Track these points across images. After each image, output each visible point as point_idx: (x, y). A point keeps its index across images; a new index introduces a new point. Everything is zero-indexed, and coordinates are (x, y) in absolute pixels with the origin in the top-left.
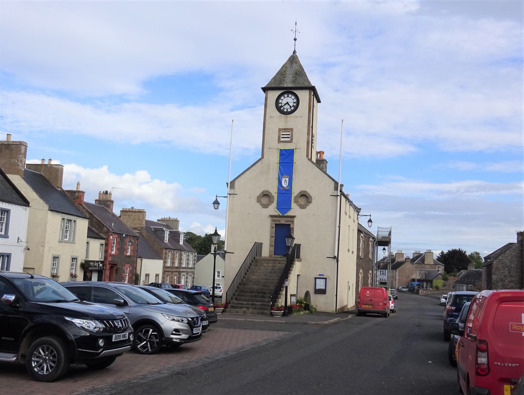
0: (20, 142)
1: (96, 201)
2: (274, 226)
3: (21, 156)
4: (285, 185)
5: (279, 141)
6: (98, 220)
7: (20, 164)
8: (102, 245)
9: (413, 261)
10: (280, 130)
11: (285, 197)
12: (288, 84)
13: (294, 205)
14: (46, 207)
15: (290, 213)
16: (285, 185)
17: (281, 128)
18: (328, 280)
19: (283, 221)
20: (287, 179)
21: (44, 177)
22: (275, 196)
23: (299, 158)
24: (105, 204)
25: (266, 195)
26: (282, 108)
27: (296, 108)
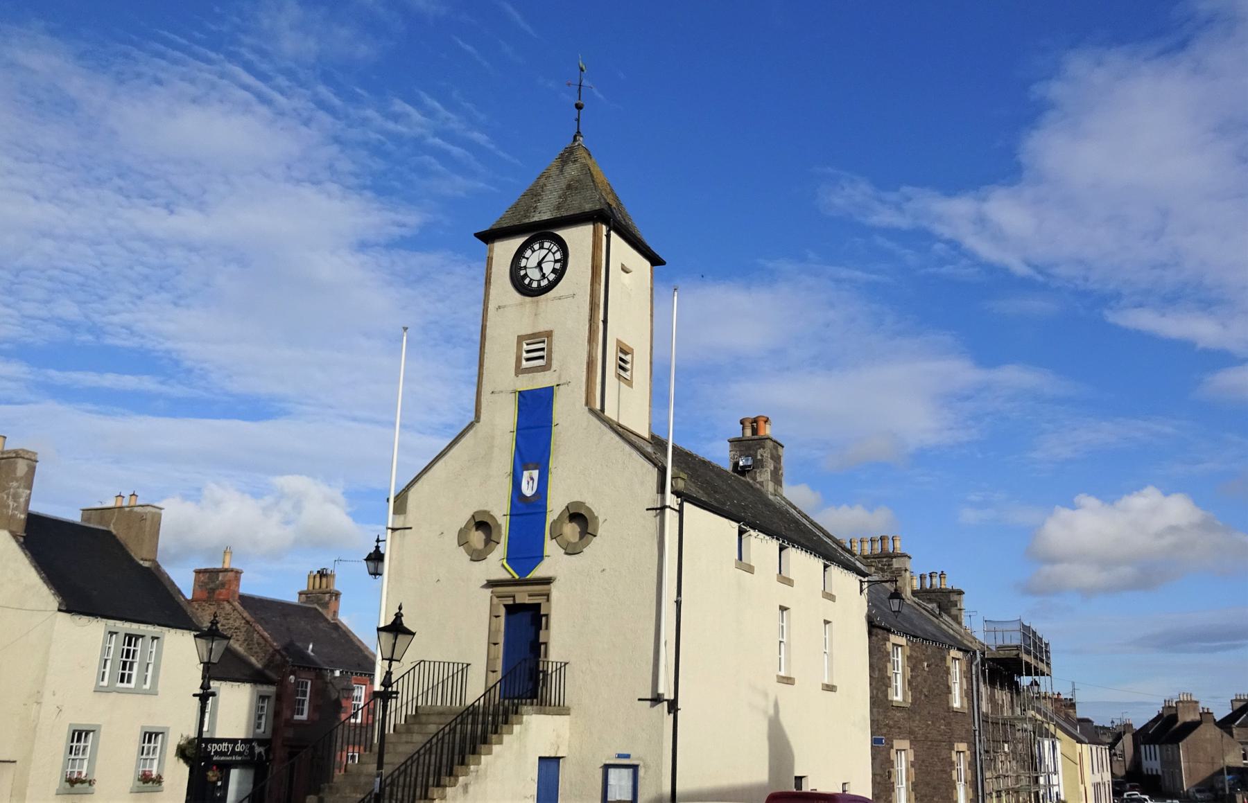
0: (16, 452)
1: (300, 594)
2: (502, 611)
3: (15, 484)
4: (528, 489)
5: (519, 371)
6: (262, 637)
7: (11, 503)
8: (262, 698)
9: (1226, 724)
10: (521, 339)
11: (527, 529)
12: (544, 214)
13: (550, 546)
14: (52, 601)
15: (539, 572)
16: (528, 489)
17: (523, 333)
18: (641, 772)
19: (523, 596)
20: (535, 473)
21: (114, 537)
22: (504, 523)
23: (568, 413)
24: (319, 601)
25: (483, 524)
26: (527, 281)
27: (560, 274)
